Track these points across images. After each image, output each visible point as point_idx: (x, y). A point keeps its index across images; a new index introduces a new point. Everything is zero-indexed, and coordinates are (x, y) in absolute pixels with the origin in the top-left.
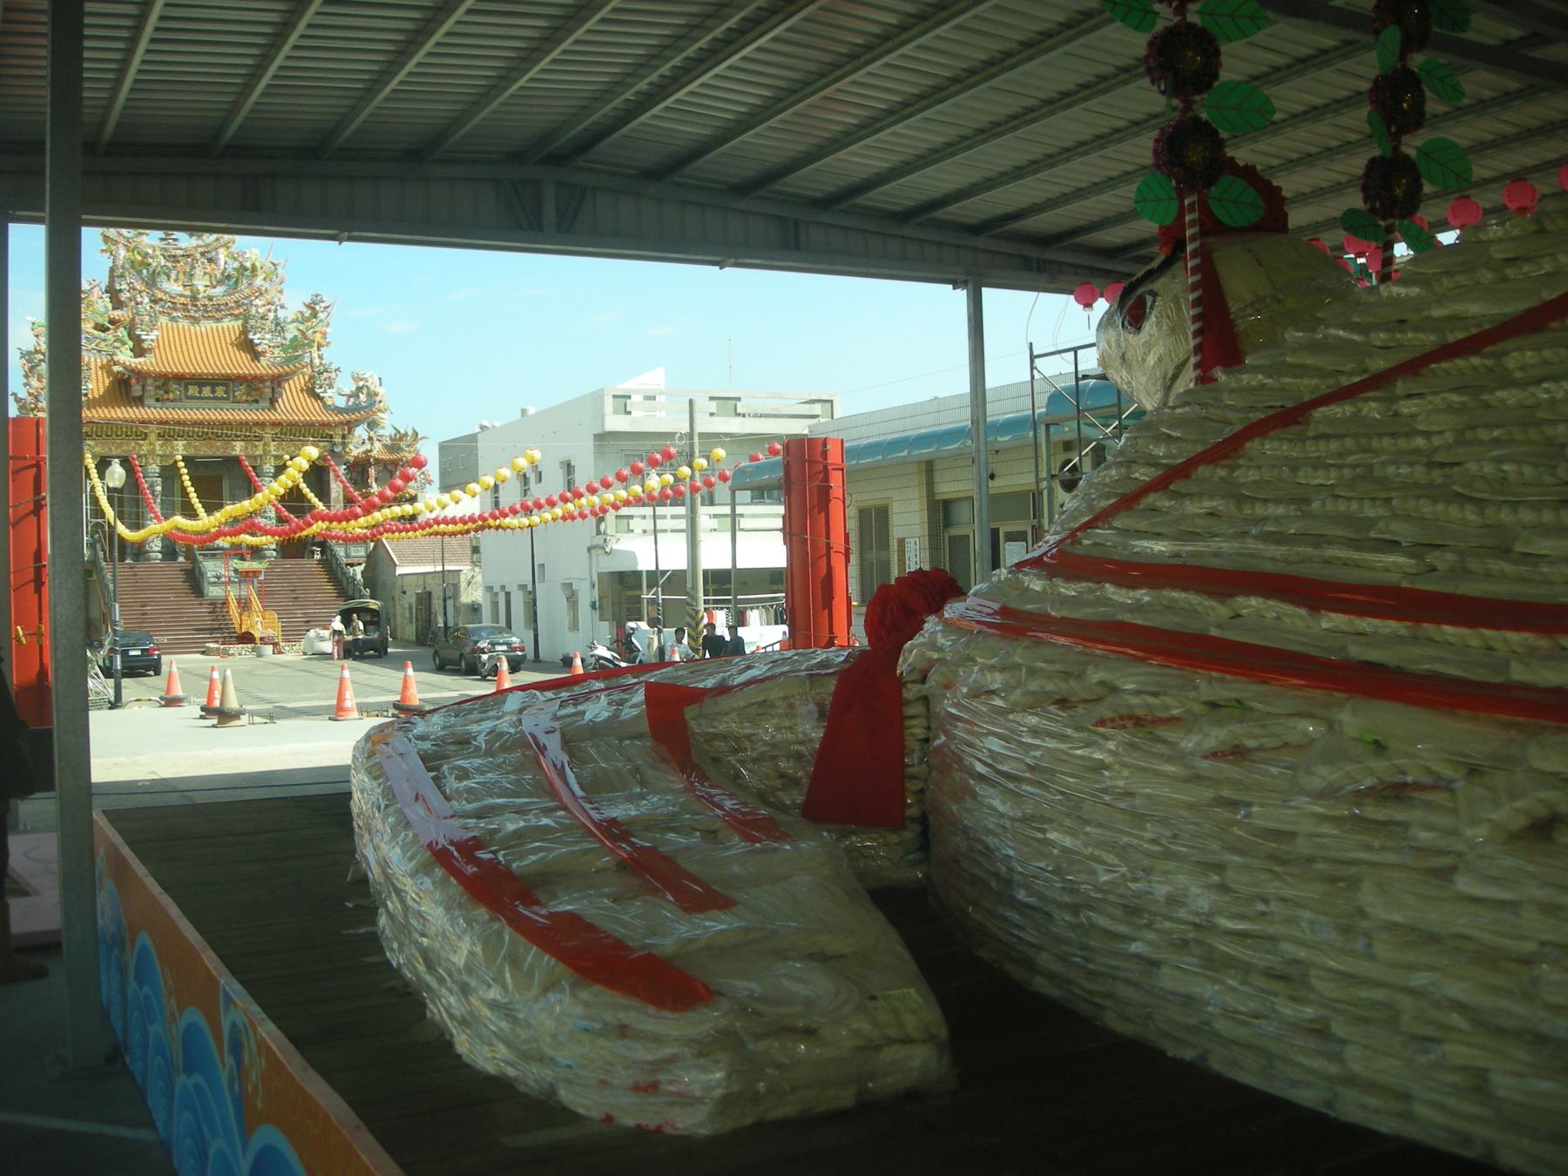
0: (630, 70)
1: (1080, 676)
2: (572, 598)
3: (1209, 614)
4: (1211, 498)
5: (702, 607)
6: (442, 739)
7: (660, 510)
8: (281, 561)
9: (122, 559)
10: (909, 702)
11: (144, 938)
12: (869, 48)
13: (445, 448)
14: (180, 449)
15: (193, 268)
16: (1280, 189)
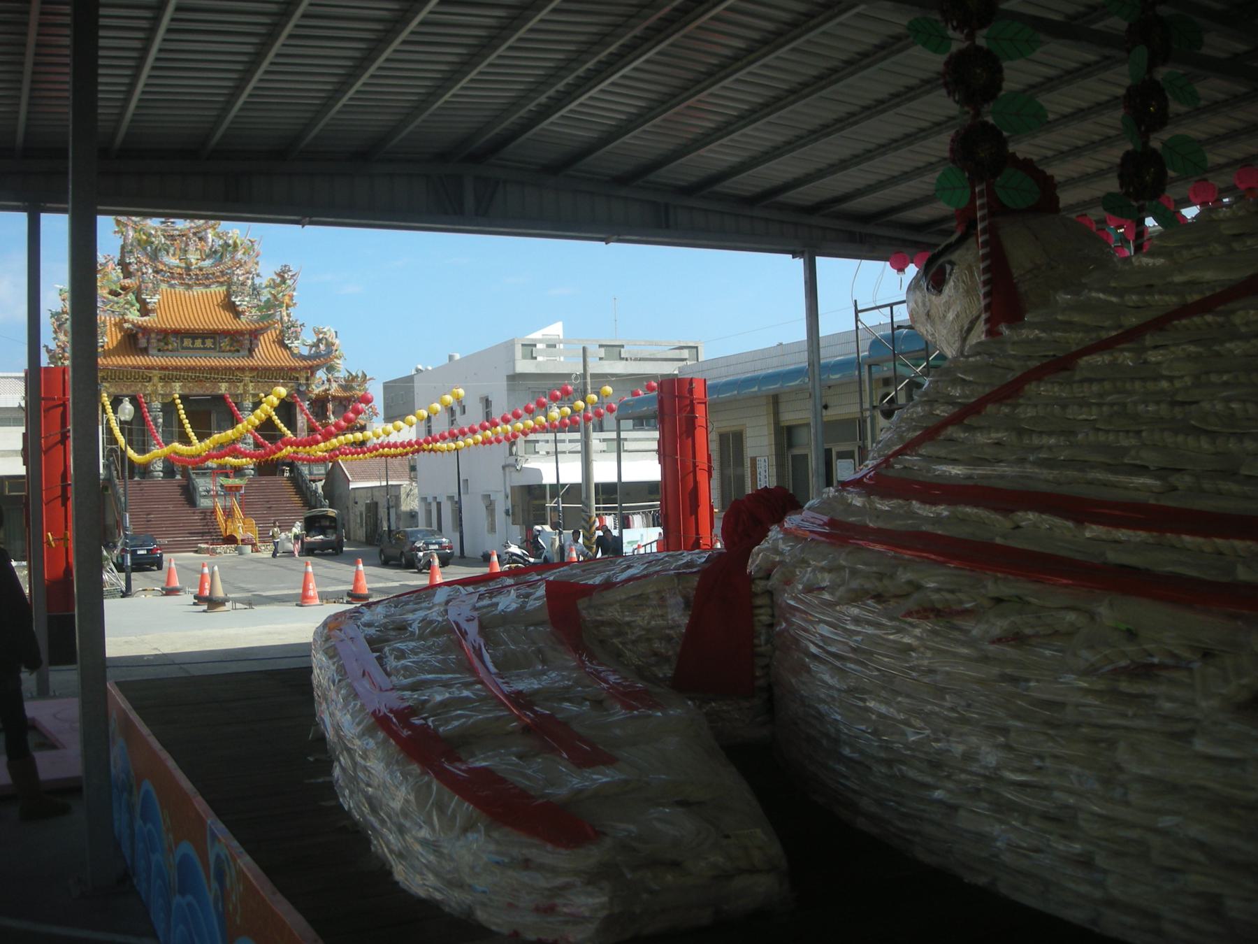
0: (533, 87)
1: (892, 576)
3: (994, 525)
4: (997, 431)
5: (594, 513)
6: (385, 626)
7: (560, 436)
8: (259, 478)
9: (131, 477)
10: (756, 595)
11: (147, 785)
12: (722, 67)
13: (388, 387)
15: (187, 245)
16: (1052, 177)
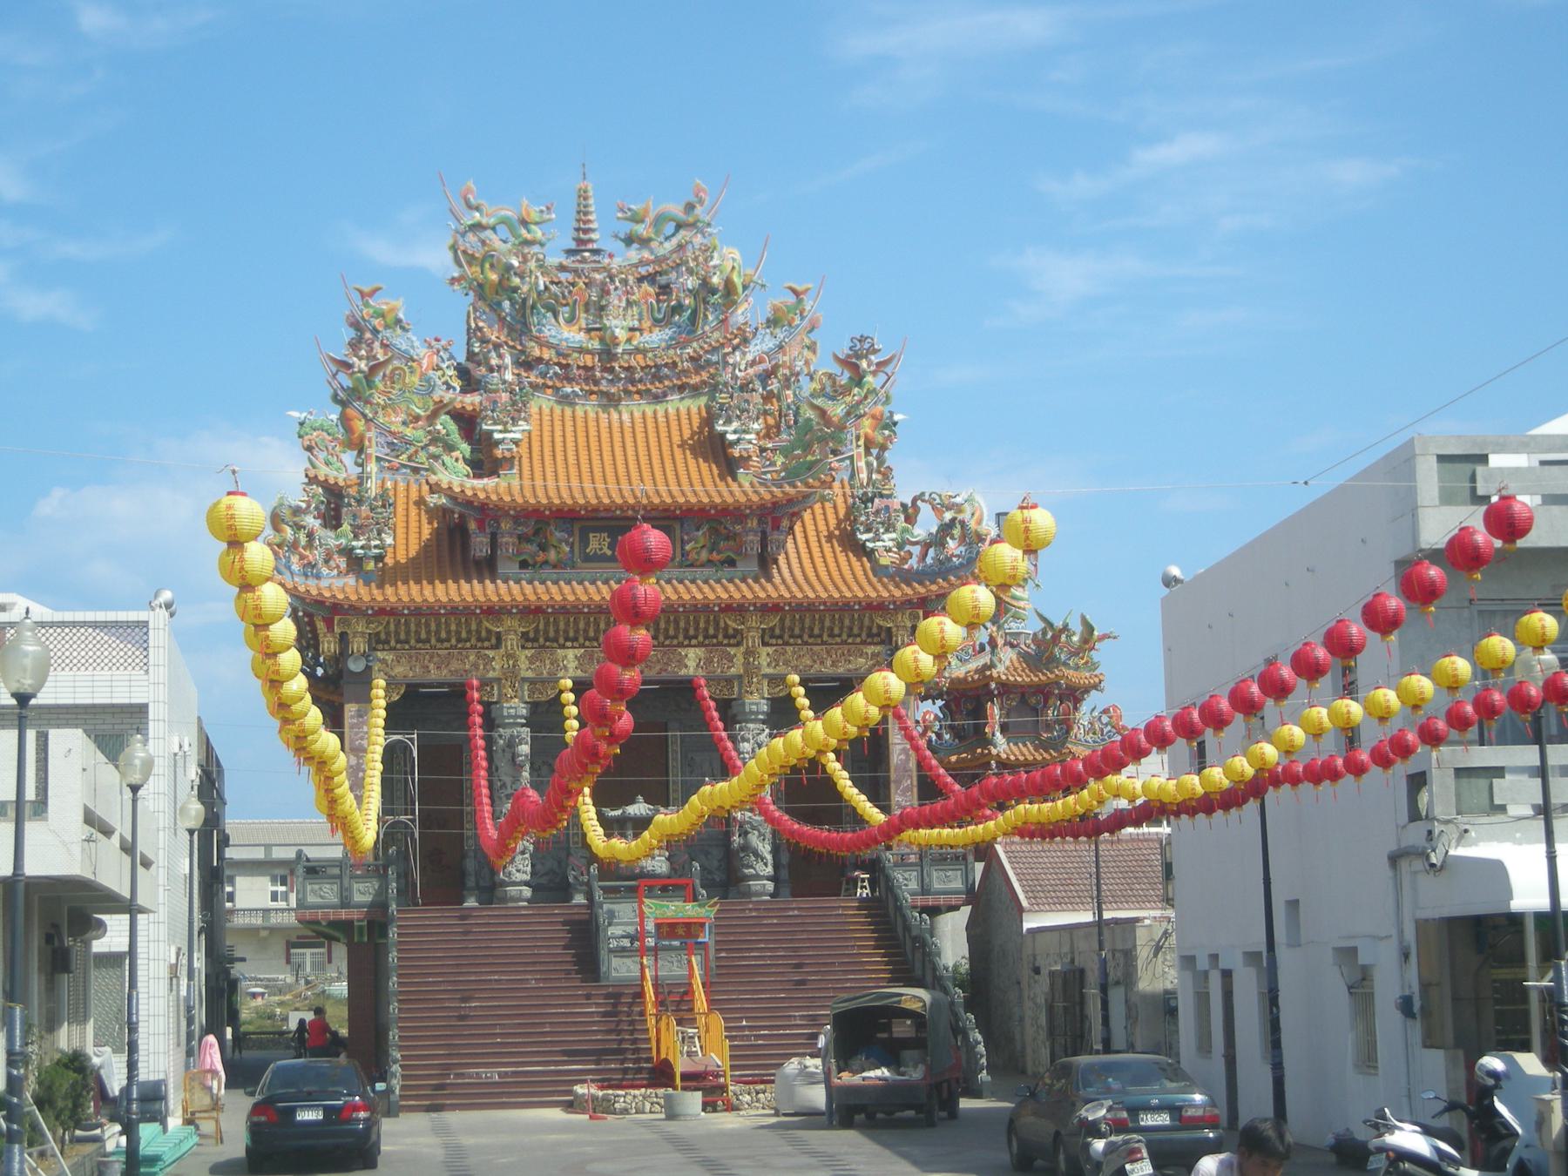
2: (1360, 986)
14: (570, 664)
15: (605, 292)
